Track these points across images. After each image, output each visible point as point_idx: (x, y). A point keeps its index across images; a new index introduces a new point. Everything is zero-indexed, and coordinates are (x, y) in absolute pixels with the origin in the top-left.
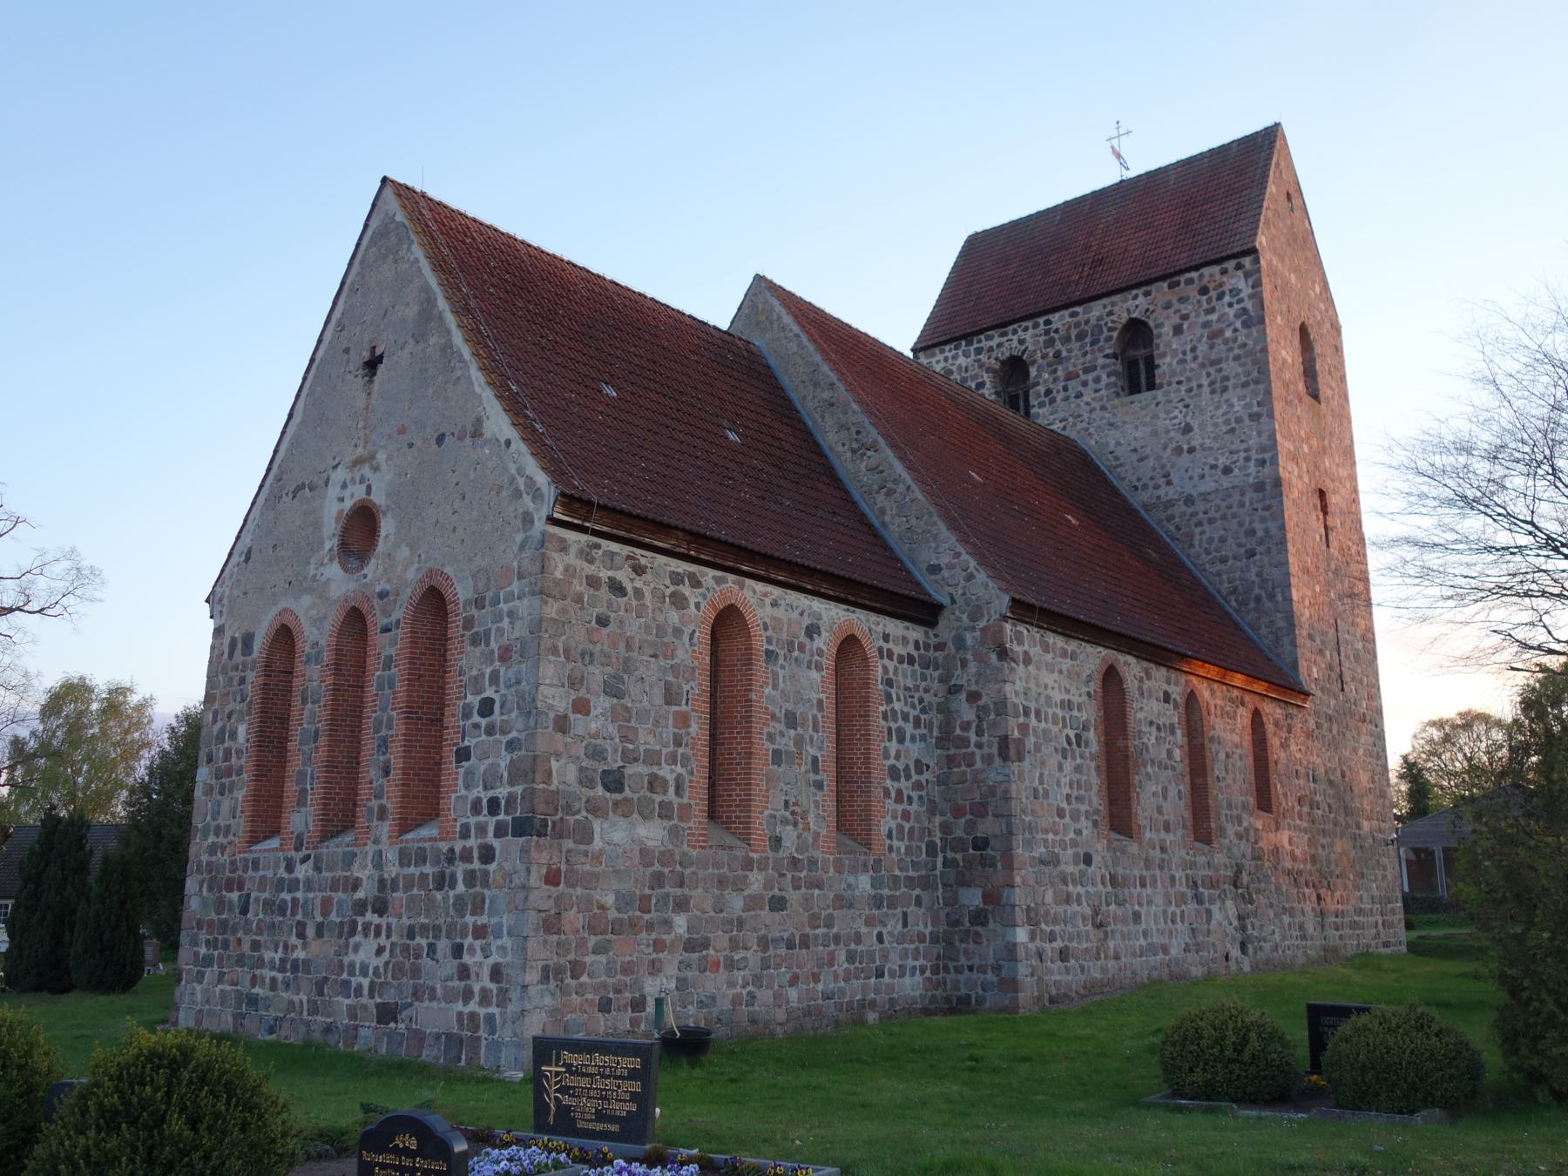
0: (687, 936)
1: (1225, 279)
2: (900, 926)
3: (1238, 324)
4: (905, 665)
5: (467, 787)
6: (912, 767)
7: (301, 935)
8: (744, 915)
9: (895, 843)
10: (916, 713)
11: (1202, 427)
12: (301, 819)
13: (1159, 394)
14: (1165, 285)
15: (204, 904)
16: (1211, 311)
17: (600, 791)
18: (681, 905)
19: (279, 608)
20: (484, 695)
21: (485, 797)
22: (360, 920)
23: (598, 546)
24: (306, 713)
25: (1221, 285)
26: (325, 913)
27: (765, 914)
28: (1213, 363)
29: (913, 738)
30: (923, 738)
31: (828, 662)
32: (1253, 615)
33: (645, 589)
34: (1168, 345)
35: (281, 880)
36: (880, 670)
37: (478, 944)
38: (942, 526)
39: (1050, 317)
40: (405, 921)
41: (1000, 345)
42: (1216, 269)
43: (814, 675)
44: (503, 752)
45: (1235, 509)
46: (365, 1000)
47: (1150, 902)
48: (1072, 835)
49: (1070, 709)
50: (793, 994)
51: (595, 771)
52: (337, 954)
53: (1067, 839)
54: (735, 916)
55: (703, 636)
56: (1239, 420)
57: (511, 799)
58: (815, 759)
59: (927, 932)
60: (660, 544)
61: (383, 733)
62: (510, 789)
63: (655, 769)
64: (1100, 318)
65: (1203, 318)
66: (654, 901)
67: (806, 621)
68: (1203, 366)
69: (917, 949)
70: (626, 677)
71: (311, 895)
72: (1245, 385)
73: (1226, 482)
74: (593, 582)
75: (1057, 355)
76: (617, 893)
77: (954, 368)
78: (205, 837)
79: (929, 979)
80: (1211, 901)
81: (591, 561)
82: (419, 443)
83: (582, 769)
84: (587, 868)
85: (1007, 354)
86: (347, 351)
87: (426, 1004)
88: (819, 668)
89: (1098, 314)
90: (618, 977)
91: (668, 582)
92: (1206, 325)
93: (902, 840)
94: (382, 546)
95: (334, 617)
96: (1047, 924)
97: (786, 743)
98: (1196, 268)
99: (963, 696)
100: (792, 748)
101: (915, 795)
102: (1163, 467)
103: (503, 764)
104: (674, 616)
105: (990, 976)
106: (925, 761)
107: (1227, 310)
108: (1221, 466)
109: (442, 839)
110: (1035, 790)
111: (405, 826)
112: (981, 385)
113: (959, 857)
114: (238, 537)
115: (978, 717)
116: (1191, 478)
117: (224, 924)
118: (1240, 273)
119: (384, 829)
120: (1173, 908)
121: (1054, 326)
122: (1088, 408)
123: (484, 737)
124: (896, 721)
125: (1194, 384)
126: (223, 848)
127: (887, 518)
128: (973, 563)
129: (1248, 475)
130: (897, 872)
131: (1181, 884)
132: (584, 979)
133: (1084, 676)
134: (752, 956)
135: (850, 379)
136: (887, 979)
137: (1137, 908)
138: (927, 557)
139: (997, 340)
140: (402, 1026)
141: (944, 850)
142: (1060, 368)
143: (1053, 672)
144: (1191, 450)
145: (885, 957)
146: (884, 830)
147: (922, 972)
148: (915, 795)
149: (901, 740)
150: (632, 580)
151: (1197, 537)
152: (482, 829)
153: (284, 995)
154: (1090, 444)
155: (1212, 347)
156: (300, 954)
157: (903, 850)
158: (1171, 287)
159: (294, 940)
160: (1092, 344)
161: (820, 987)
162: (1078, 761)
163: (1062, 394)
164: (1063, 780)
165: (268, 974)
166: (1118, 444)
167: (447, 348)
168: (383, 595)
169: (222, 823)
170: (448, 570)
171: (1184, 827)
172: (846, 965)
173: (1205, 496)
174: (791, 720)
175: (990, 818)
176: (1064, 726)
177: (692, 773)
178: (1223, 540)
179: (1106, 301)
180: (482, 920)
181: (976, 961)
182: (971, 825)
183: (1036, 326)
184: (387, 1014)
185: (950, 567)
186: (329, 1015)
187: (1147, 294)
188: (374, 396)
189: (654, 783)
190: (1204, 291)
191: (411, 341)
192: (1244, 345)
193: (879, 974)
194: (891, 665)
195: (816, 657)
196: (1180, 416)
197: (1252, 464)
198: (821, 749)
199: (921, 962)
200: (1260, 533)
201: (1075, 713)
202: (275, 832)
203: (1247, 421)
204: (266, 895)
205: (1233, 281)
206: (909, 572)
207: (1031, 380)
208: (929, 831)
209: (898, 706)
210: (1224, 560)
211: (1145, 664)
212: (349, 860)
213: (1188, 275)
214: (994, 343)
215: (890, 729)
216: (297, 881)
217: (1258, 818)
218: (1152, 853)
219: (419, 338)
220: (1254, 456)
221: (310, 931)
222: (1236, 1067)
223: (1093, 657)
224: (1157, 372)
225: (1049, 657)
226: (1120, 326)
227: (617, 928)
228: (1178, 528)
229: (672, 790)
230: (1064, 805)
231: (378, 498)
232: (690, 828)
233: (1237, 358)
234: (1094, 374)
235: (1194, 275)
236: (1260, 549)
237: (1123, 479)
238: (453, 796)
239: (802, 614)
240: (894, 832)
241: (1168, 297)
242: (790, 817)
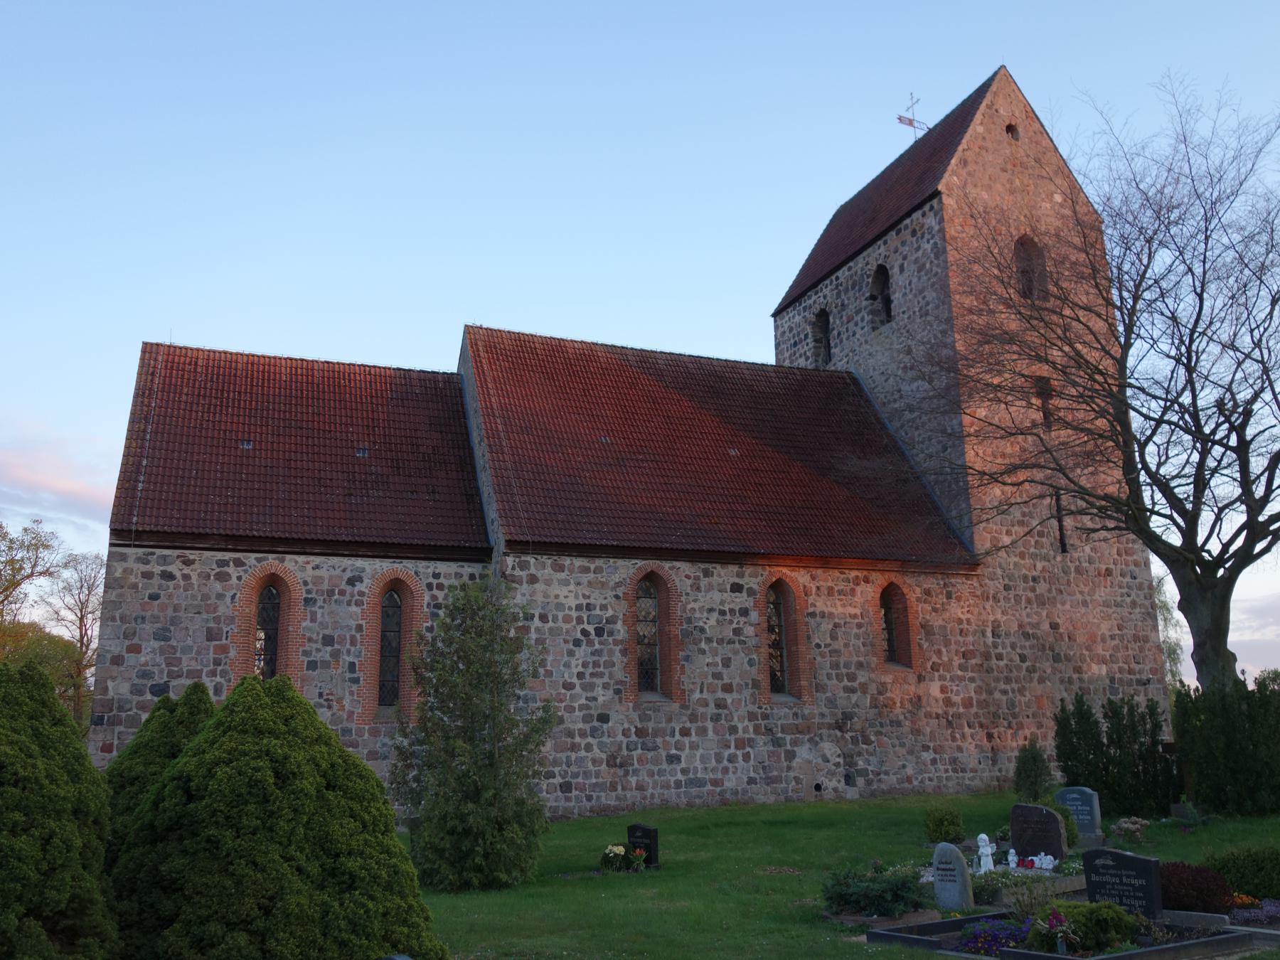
14: (893, 233)
23: (153, 554)
33: (191, 574)
43: (354, 609)
51: (145, 685)
60: (201, 546)
67: (348, 574)
70: (172, 628)
74: (147, 575)
83: (133, 685)
88: (358, 604)
89: (860, 265)
104: (218, 587)
139: (814, 298)
154: (859, 372)
160: (860, 290)
192: (937, 274)
211: (703, 566)
217: (885, 672)
223: (626, 570)
224: (893, 306)
225: (562, 576)
226: (872, 273)
235: (908, 221)
239: (344, 571)
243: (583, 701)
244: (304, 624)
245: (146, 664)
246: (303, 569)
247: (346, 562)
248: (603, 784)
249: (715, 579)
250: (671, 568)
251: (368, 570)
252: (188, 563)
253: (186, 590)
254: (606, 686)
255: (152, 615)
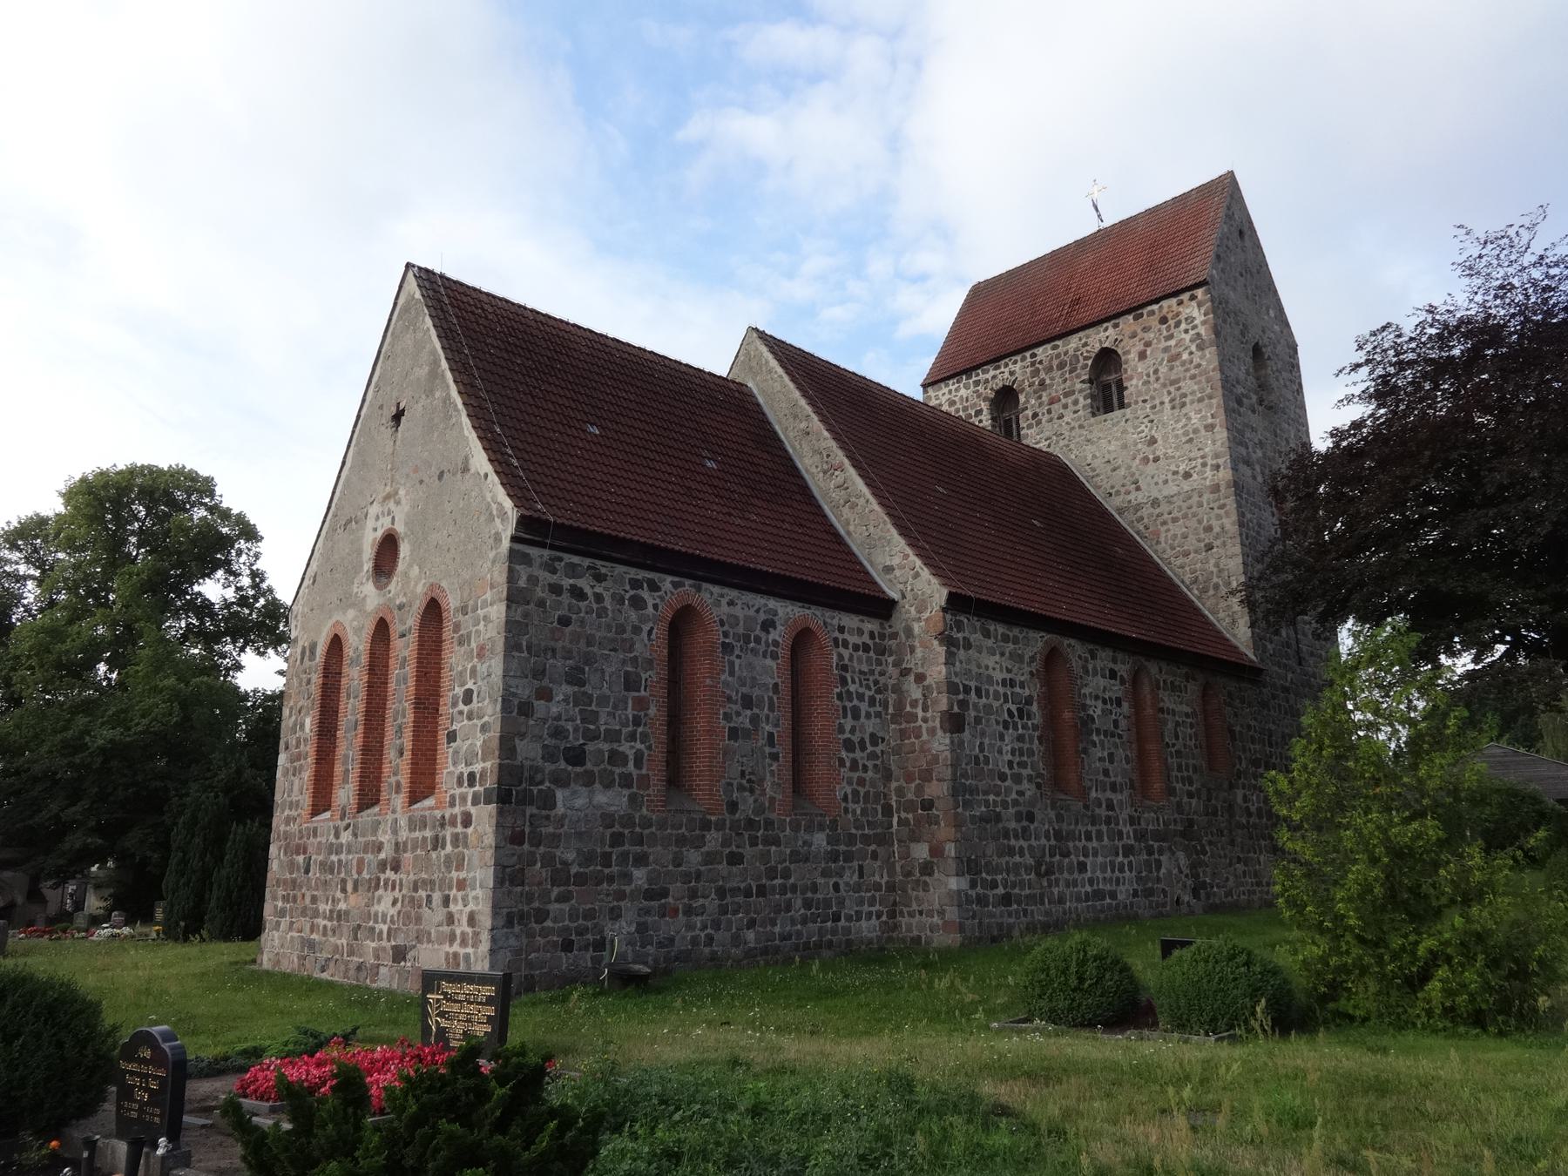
0: (646, 886)
1: (1181, 309)
2: (856, 877)
3: (1193, 348)
4: (861, 653)
5: (455, 764)
6: (867, 741)
7: (344, 890)
8: (702, 868)
9: (851, 806)
10: (872, 693)
11: (1166, 439)
12: (345, 794)
13: (1128, 411)
14: (1130, 317)
15: (281, 865)
16: (1171, 337)
17: (562, 765)
18: (641, 860)
19: (334, 620)
20: (467, 687)
21: (466, 771)
22: (382, 877)
23: (560, 559)
24: (350, 706)
25: (1178, 314)
26: (359, 872)
27: (723, 867)
28: (1173, 383)
29: (868, 716)
30: (878, 715)
31: (784, 652)
32: (1213, 601)
33: (605, 594)
34: (1135, 369)
35: (332, 844)
36: (835, 657)
37: (460, 894)
38: (894, 532)
39: (1035, 351)
40: (412, 877)
41: (994, 377)
42: (1174, 301)
43: (769, 662)
44: (479, 735)
45: (1194, 509)
46: (384, 943)
47: (1095, 854)
48: (1014, 796)
49: (1012, 686)
50: (750, 936)
52: (367, 905)
53: (1009, 800)
54: (693, 870)
55: (660, 632)
56: (1196, 431)
57: (483, 773)
58: (771, 735)
59: (883, 882)
61: (399, 721)
62: (482, 765)
63: (615, 746)
64: (1077, 350)
65: (1163, 344)
66: (614, 857)
67: (762, 617)
68: (1164, 385)
69: (874, 896)
71: (350, 857)
72: (1200, 400)
73: (1186, 486)
74: (556, 589)
75: (1042, 383)
76: (579, 851)
77: (956, 399)
78: (283, 812)
79: (886, 923)
80: (1161, 852)
81: (554, 571)
82: (426, 480)
83: (545, 747)
84: (551, 830)
85: (1001, 385)
86: (381, 407)
87: (425, 946)
88: (774, 656)
89: (1074, 345)
90: (581, 922)
91: (628, 588)
92: (1166, 349)
93: (858, 802)
94: (401, 566)
95: (369, 626)
96: (988, 874)
97: (744, 720)
98: (1157, 301)
99: (912, 678)
100: (749, 726)
101: (870, 764)
102: (1133, 475)
103: (479, 744)
104: (633, 615)
105: (936, 919)
106: (880, 734)
107: (1183, 336)
108: (1182, 472)
109: (437, 808)
110: (977, 758)
111: (414, 798)
112: (979, 413)
113: (910, 816)
114: (308, 565)
115: (924, 695)
116: (1157, 484)
117: (294, 881)
118: (1194, 303)
119: (399, 800)
120: (1120, 859)
121: (1038, 359)
122: (1068, 427)
123: (466, 722)
124: (851, 701)
125: (1157, 402)
126: (295, 819)
127: (851, 528)
128: (918, 562)
129: (1205, 479)
130: (853, 831)
131: (1128, 837)
132: (548, 923)
133: (1027, 659)
134: (711, 903)
135: (825, 412)
136: (843, 923)
137: (1082, 858)
138: (883, 559)
139: (992, 373)
140: (409, 964)
141: (898, 812)
142: (1044, 394)
143: (994, 654)
144: (1156, 460)
145: (841, 903)
146: (839, 795)
147: (879, 916)
148: (870, 764)
149: (856, 716)
150: (592, 587)
151: (1163, 535)
152: (463, 798)
153: (332, 939)
154: (1069, 459)
155: (1171, 368)
156: (342, 906)
157: (858, 812)
158: (1136, 318)
159: (339, 894)
160: (1071, 372)
161: (777, 929)
162: (1020, 731)
163: (1047, 417)
164: (1005, 749)
165: (322, 922)
166: (1094, 457)
167: (447, 399)
168: (401, 607)
169: (294, 799)
170: (444, 584)
171: (1132, 787)
172: (802, 911)
173: (1169, 499)
174: (747, 702)
175: (935, 782)
176: (1006, 701)
177: (649, 748)
178: (1185, 537)
179: (1081, 334)
180: (463, 875)
181: (925, 907)
182: (920, 789)
183: (1024, 359)
184: (399, 954)
185: (902, 567)
186: (361, 956)
187: (1116, 326)
188: (398, 443)
189: (616, 758)
190: (1164, 320)
191: (424, 397)
192: (1199, 366)
193: (836, 918)
194: (846, 653)
195: (772, 648)
196: (1146, 430)
197: (1208, 468)
198: (776, 725)
199: (877, 907)
200: (1217, 529)
201: (1017, 690)
202: (327, 808)
203: (1203, 432)
204: (321, 858)
205: (1188, 311)
206: (867, 573)
207: (1021, 406)
208: (885, 795)
209: (852, 688)
210: (1186, 554)
212: (375, 827)
213: (1149, 308)
214: (989, 376)
215: (845, 708)
216: (342, 845)
218: (1097, 811)
219: (430, 393)
220: (1210, 462)
221: (349, 887)
222: (1078, 996)
223: (1037, 642)
225: (990, 643)
227: (581, 879)
228: (1146, 528)
229: (631, 764)
230: (1007, 770)
231: (400, 528)
232: (649, 795)
233: (1193, 377)
234: (1073, 397)
235: (1155, 307)
236: (1216, 543)
237: (1100, 487)
238: (445, 771)
239: (758, 611)
240: (850, 796)
241: (1133, 328)
242: (748, 785)
243: (1014, 796)
244: (723, 677)
245: (558, 718)
246: (718, 604)
247: (759, 601)
248: (1035, 895)
249: (1099, 664)
250: (1069, 645)
251: (780, 612)
252: (599, 578)
253: (599, 616)
254: (1030, 778)
255: (563, 647)
